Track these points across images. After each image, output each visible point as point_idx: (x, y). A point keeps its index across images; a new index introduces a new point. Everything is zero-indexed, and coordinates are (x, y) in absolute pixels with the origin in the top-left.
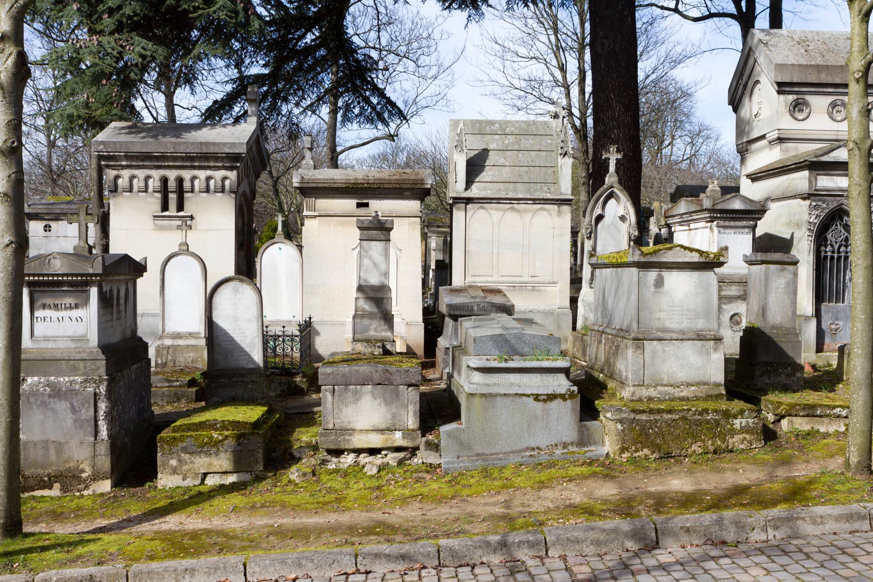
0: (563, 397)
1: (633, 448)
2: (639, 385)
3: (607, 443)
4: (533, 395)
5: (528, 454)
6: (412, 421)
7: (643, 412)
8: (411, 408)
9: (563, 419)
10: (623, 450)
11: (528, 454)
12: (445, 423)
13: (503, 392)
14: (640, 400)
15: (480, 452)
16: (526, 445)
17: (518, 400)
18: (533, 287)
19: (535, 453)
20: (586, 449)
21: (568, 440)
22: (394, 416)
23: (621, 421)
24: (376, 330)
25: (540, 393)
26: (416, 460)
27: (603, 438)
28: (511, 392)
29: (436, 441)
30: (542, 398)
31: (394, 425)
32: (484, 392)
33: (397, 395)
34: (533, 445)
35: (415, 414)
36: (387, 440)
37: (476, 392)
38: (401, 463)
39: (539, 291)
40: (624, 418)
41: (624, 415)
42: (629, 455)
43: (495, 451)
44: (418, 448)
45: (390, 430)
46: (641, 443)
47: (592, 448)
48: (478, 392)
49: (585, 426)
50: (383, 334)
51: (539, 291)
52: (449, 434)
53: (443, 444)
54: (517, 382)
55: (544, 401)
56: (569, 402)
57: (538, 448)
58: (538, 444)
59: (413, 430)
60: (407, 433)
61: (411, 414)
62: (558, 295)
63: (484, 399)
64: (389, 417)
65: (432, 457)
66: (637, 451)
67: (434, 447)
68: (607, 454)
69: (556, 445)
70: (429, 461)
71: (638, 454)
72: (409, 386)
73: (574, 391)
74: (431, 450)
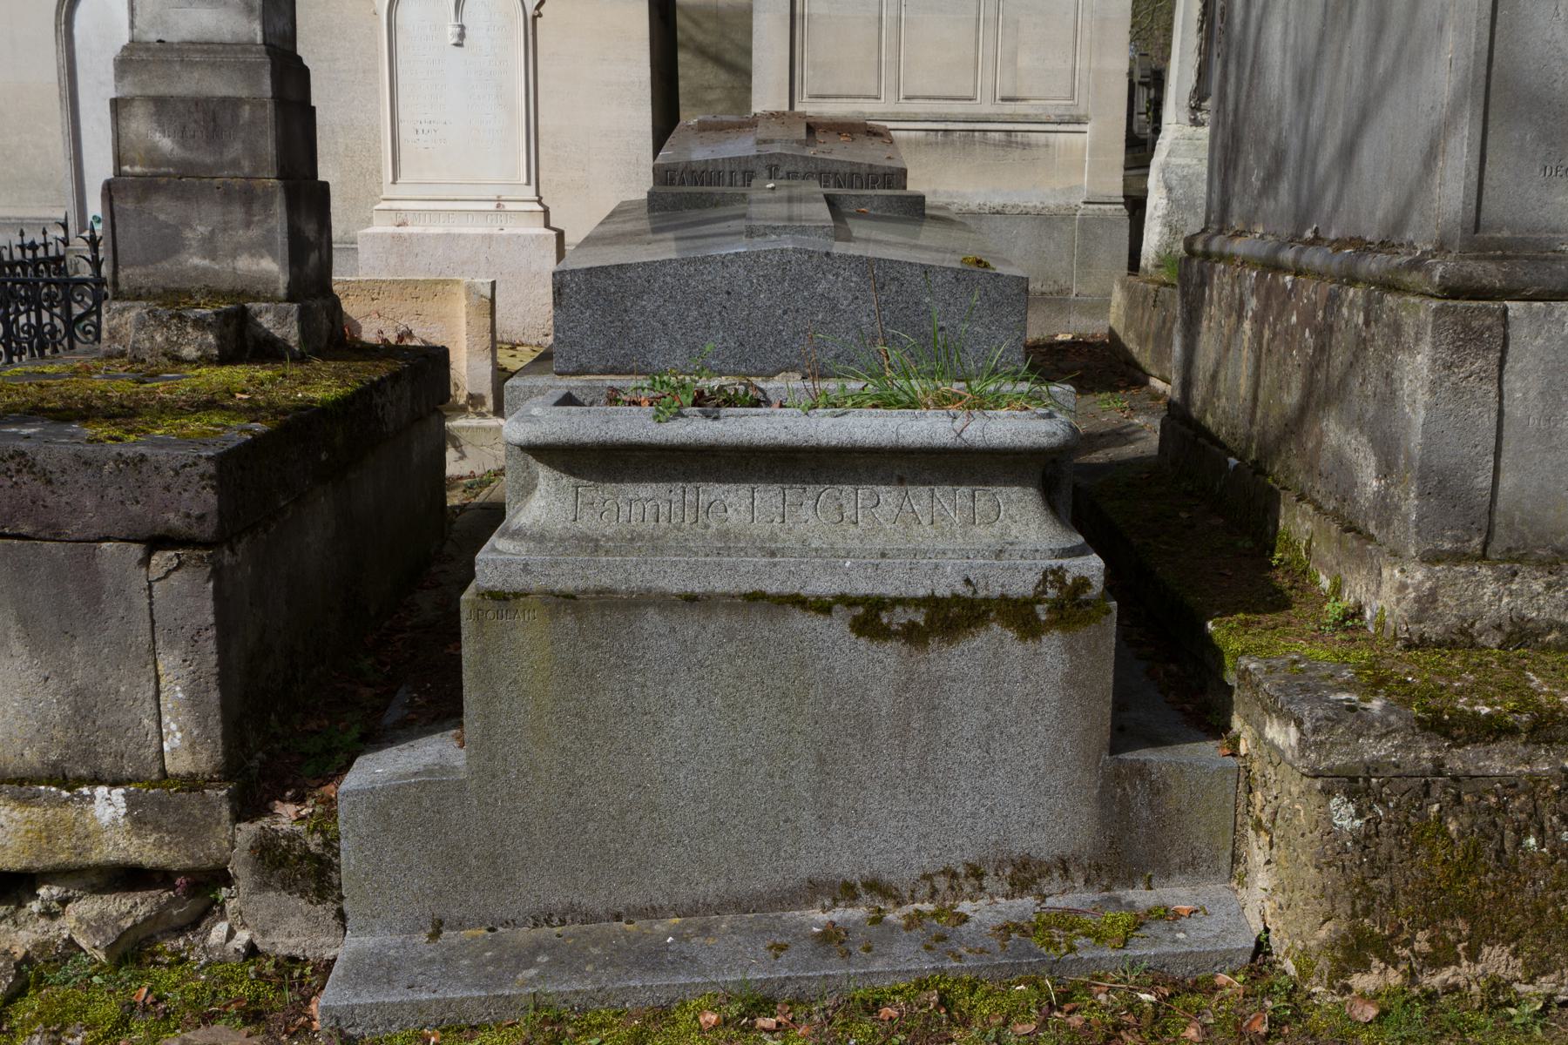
0: (1019, 615)
1: (1422, 943)
2: (1457, 557)
3: (1262, 879)
4: (846, 600)
5: (818, 917)
6: (182, 739)
7: (1493, 731)
8: (168, 662)
9: (1014, 736)
10: (1355, 951)
11: (818, 917)
12: (375, 738)
13: (674, 582)
14: (1462, 640)
15: (557, 900)
16: (806, 868)
17: (761, 627)
18: (1007, 137)
19: (857, 913)
20: (1141, 897)
21: (1040, 844)
22: (83, 707)
23: (1354, 784)
24: (209, 247)
25: (889, 589)
26: (218, 932)
27: (1237, 841)
28: (720, 585)
29: (314, 843)
30: (900, 617)
31: (88, 753)
32: (568, 584)
33: (93, 592)
34: (845, 867)
35: (194, 698)
36: (48, 834)
37: (519, 582)
38: (132, 950)
39: (1026, 146)
40: (1373, 768)
41: (1375, 750)
42: (1395, 978)
43: (636, 899)
44: (220, 876)
45: (67, 778)
46: (1469, 912)
47: (1177, 894)
48: (535, 584)
49: (1141, 771)
50: (244, 264)
51: (1026, 146)
52: (384, 801)
53: (349, 859)
54: (761, 528)
55: (913, 635)
56: (1052, 646)
57: (875, 886)
58: (879, 865)
59: (191, 783)
60: (156, 794)
61: (174, 693)
62: (1084, 166)
63: (568, 621)
64: (58, 712)
65: (294, 923)
66: (1436, 961)
67: (309, 873)
68: (1261, 947)
69: (976, 873)
70: (282, 943)
71: (1447, 974)
72: (155, 543)
73: (1083, 583)
74: (288, 886)
